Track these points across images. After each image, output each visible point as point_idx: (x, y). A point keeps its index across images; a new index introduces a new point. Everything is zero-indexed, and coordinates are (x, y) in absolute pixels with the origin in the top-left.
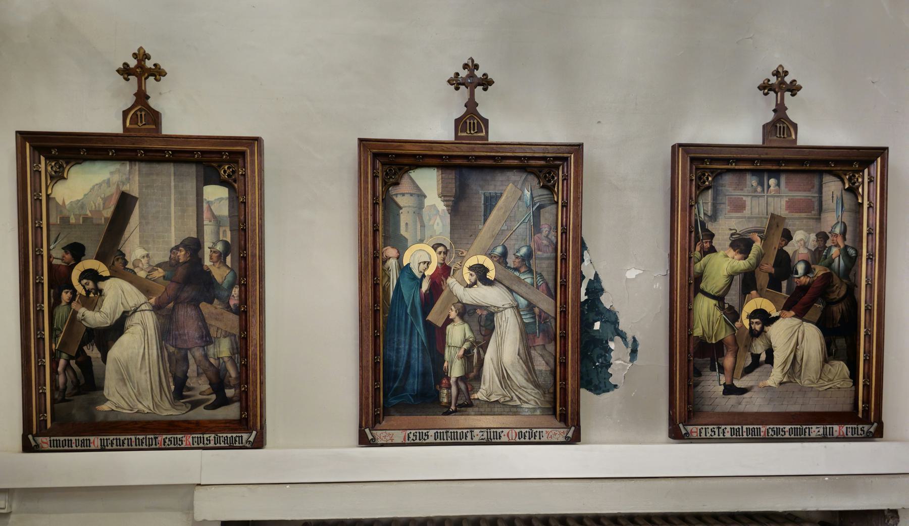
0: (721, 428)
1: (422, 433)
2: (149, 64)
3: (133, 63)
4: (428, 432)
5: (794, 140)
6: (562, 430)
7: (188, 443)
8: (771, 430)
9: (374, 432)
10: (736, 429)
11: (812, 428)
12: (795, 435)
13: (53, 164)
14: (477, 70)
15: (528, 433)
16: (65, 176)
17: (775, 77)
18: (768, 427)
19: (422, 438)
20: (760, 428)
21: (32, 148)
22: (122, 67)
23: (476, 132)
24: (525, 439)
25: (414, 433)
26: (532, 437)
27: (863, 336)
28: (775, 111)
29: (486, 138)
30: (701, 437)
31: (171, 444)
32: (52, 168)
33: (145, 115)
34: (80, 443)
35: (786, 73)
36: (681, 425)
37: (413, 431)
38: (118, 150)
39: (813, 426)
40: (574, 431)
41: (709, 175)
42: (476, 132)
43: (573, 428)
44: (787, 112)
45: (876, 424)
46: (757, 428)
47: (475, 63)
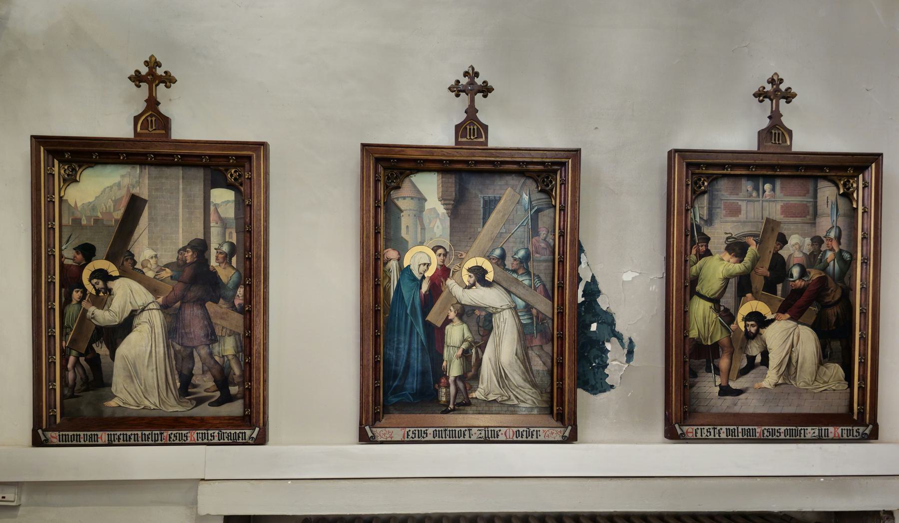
0: (716, 428)
1: (421, 431)
2: (160, 71)
3: (144, 70)
4: (427, 430)
6: (559, 430)
9: (374, 429)
10: (732, 430)
11: (807, 429)
13: (66, 167)
15: (525, 432)
16: (78, 179)
17: (771, 84)
18: (763, 428)
19: (421, 436)
21: (46, 152)
24: (522, 437)
25: (707, 430)
26: (529, 436)
28: (770, 117)
29: (486, 143)
31: (176, 439)
32: (65, 171)
33: (155, 120)
34: (88, 438)
36: (677, 426)
37: (412, 429)
39: (808, 428)
41: (704, 180)
42: (476, 138)
43: (570, 428)
45: (871, 426)
46: (752, 429)
47: (475, 70)
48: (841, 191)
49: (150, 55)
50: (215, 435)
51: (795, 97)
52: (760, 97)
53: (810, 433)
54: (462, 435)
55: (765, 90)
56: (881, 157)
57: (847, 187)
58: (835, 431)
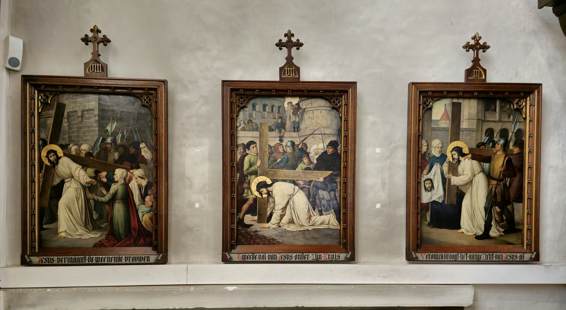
5: (484, 79)
7: (325, 258)
8: (44, 259)
9: (416, 254)
11: (309, 255)
12: (139, 261)
13: (42, 95)
14: (293, 37)
15: (252, 256)
17: (474, 40)
19: (289, 258)
20: (276, 255)
21: (30, 85)
22: (84, 37)
23: (288, 75)
24: (144, 261)
27: (527, 199)
30: (467, 260)
31: (47, 262)
34: (261, 257)
35: (293, 35)
36: (413, 253)
38: (293, 91)
39: (309, 254)
40: (535, 255)
42: (288, 75)
43: (350, 253)
44: (480, 62)
45: (535, 253)
46: (475, 255)
48: (515, 107)
49: (94, 25)
50: (292, 256)
51: (489, 48)
52: (466, 48)
53: (311, 257)
54: (143, 259)
55: (469, 44)
56: (541, 86)
57: (519, 104)
58: (325, 257)
